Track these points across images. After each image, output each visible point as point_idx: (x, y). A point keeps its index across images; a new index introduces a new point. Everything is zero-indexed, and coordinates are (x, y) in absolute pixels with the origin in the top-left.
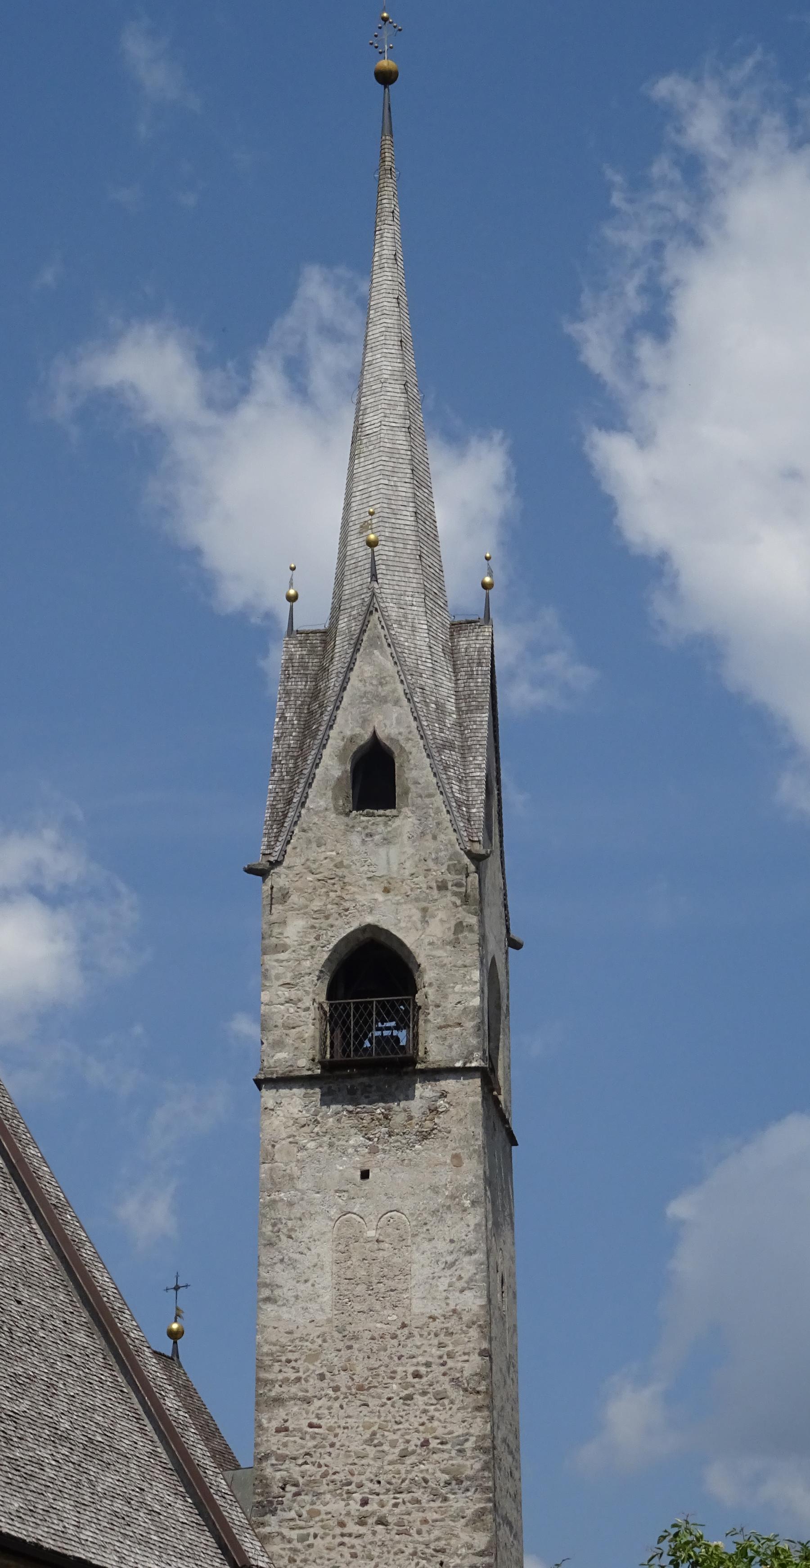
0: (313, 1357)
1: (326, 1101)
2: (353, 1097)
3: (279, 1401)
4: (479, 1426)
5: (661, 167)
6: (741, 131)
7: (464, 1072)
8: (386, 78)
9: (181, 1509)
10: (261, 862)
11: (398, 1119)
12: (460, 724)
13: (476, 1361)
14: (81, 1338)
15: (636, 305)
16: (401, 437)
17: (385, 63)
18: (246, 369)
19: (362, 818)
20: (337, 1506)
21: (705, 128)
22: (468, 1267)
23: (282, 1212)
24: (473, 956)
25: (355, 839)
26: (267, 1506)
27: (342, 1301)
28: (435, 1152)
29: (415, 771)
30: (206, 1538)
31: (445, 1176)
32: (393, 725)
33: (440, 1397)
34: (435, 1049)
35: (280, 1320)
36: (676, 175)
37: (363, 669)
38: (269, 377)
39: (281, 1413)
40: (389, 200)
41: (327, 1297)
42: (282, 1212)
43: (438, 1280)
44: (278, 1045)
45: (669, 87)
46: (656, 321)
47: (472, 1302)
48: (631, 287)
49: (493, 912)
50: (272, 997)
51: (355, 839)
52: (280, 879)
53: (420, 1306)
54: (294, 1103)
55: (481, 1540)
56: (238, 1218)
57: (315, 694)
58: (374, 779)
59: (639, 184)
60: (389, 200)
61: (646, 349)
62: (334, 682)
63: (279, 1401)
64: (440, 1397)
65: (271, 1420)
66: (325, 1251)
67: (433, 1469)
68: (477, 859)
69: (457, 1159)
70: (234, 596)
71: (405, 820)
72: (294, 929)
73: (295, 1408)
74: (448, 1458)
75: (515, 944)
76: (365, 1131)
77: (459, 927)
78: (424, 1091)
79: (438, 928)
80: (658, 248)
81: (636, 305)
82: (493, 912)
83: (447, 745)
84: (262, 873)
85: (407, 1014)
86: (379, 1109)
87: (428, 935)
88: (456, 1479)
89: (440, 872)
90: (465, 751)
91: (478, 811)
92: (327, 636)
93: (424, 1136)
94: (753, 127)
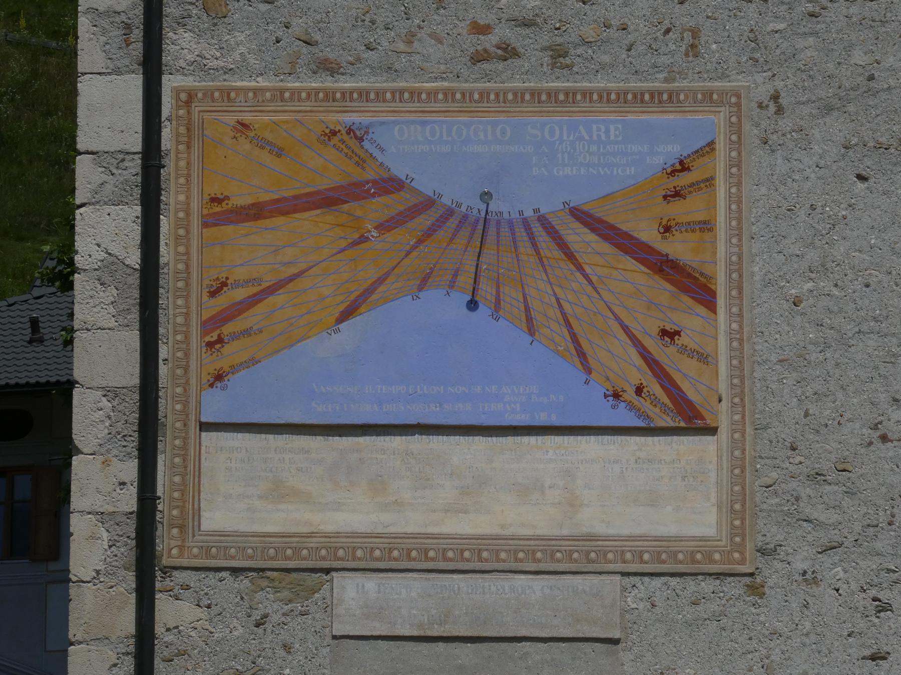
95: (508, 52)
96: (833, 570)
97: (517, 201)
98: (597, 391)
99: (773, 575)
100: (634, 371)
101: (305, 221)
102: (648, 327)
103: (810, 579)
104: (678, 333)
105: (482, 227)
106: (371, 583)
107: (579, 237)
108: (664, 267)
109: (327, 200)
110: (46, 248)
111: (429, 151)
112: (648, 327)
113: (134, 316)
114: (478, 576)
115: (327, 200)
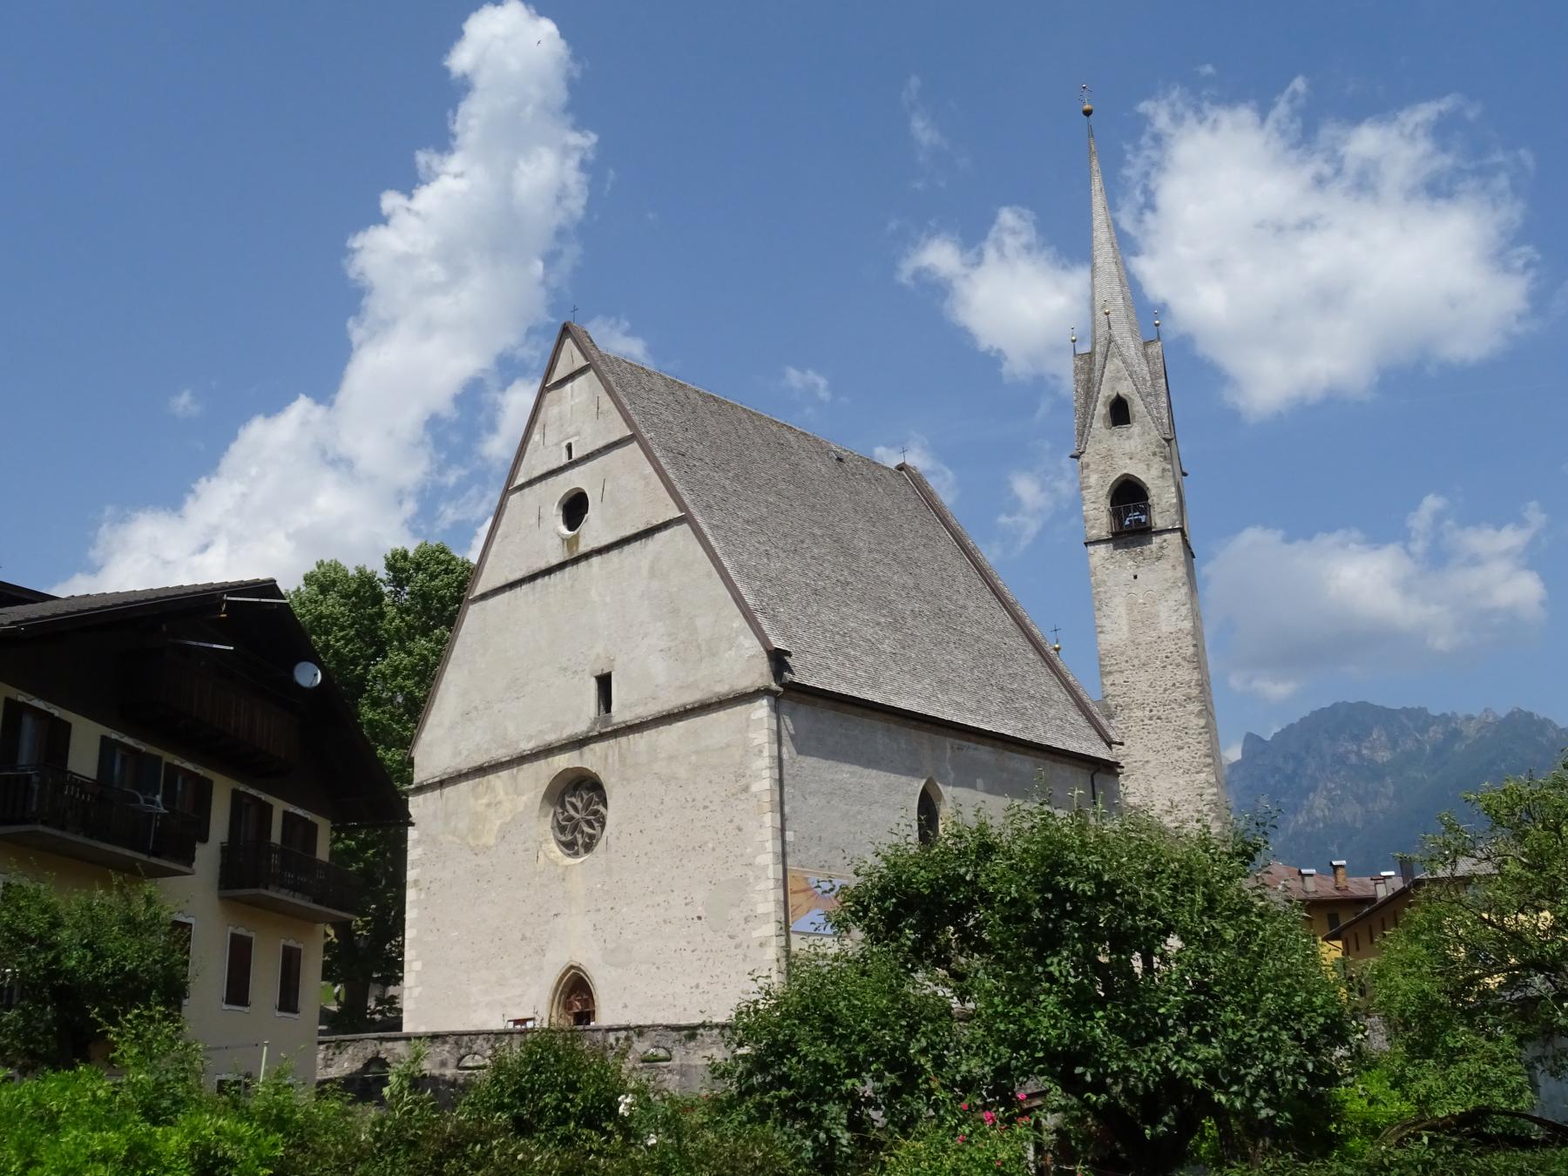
0: (1122, 654)
1: (1116, 548)
2: (1126, 546)
3: (1110, 673)
4: (1196, 676)
5: (1145, 140)
6: (1177, 119)
7: (1173, 530)
8: (1088, 113)
9: (1082, 721)
10: (1075, 452)
11: (1147, 552)
12: (1153, 385)
13: (1191, 650)
14: (1031, 656)
15: (1141, 200)
16: (1113, 267)
17: (1087, 107)
18: (981, 255)
19: (1116, 429)
20: (1139, 714)
21: (1162, 120)
22: (1184, 611)
23: (1102, 596)
24: (1171, 481)
25: (1115, 438)
26: (1110, 717)
27: (1132, 629)
28: (1163, 565)
29: (1137, 407)
30: (1093, 732)
31: (1170, 574)
32: (1125, 389)
33: (1178, 665)
34: (1159, 521)
35: (1106, 640)
36: (1151, 143)
37: (1110, 367)
38: (991, 254)
39: (1111, 678)
40: (1095, 165)
41: (1125, 629)
42: (1102, 596)
43: (1171, 616)
44: (1092, 527)
45: (1145, 107)
46: (1150, 205)
47: (1187, 625)
48: (1137, 192)
49: (1176, 462)
50: (1088, 508)
51: (1115, 438)
52: (1085, 459)
53: (1165, 628)
54: (1102, 551)
55: (1202, 722)
56: (1087, 602)
57: (1089, 380)
58: (1120, 412)
59: (1138, 148)
60: (1095, 165)
61: (1148, 216)
62: (1097, 374)
63: (1110, 673)
64: (1178, 665)
65: (1108, 681)
66: (1122, 610)
67: (1178, 695)
68: (1168, 441)
69: (1174, 567)
70: (984, 344)
71: (1135, 429)
72: (1093, 479)
73: (1117, 675)
74: (1185, 690)
75: (1185, 474)
76: (1133, 559)
77: (1164, 470)
78: (1156, 540)
79: (1155, 471)
80: (1147, 175)
81: (1141, 200)
82: (1176, 462)
83: (1149, 394)
84: (1077, 457)
85: (1146, 510)
86: (1138, 549)
87: (1150, 475)
88: (1189, 698)
89: (1153, 448)
90: (1157, 396)
91: (1165, 420)
92: (1091, 354)
93: (1159, 559)
94: (1182, 117)
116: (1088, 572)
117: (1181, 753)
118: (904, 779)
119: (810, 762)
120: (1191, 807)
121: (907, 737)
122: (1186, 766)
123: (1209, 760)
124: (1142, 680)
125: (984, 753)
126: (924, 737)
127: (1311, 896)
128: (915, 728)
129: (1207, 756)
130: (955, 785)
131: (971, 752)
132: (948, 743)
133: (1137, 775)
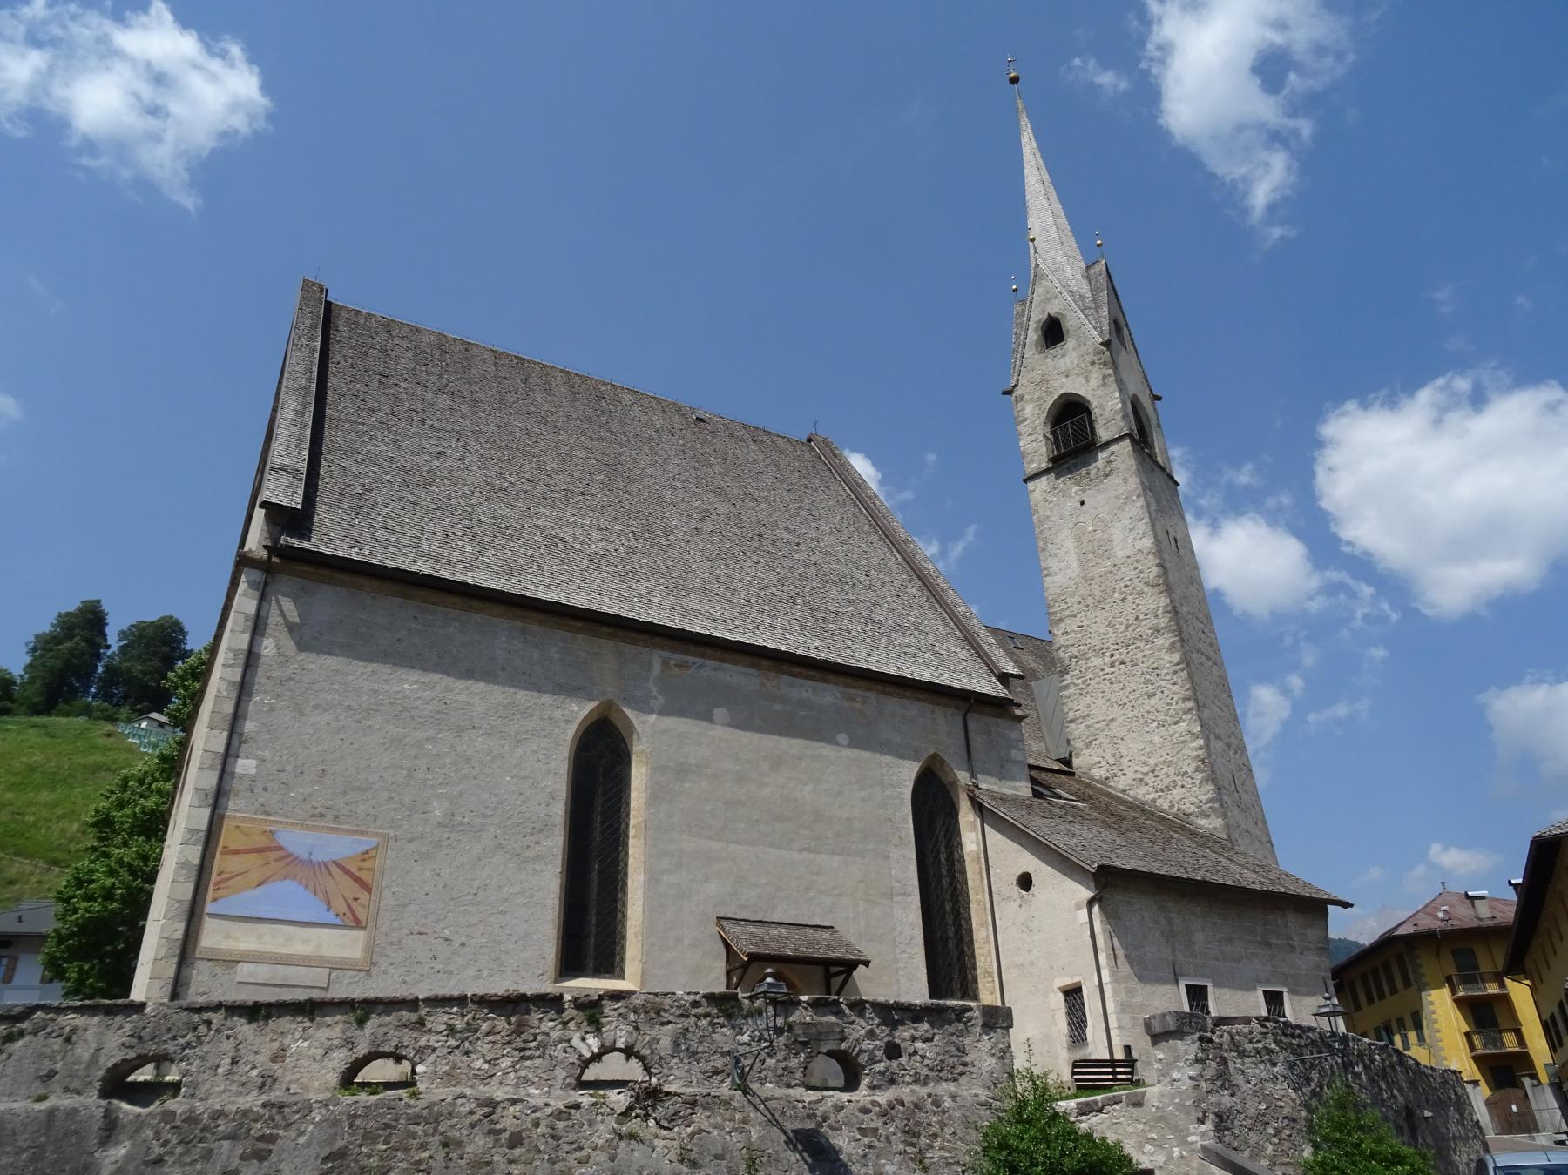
2: (1070, 471)
7: (1120, 438)
8: (1014, 81)
12: (1094, 300)
20: (1098, 662)
23: (1047, 534)
25: (1049, 361)
27: (1082, 563)
35: (1053, 584)
39: (1063, 625)
40: (1025, 121)
44: (1032, 461)
52: (1018, 392)
53: (1120, 553)
54: (1043, 483)
60: (1025, 121)
63: (1061, 620)
66: (1070, 545)
71: (1070, 343)
73: (1068, 621)
74: (1150, 622)
75: (1158, 398)
77: (1104, 377)
86: (1083, 471)
88: (1157, 631)
90: (1097, 308)
93: (1107, 475)
95: (322, 815)
96: (392, 970)
97: (319, 857)
98: (332, 913)
99: (374, 971)
100: (344, 909)
101: (250, 856)
102: (350, 898)
103: (385, 972)
104: (849, 966)
105: (311, 864)
106: (252, 966)
107: (334, 869)
108: (357, 880)
109: (259, 851)
110: (1161, 1056)
111: (296, 840)
112: (350, 898)
113: (193, 879)
114: (963, 742)
115: (259, 851)
116: (1026, 509)
117: (1153, 701)
118: (547, 699)
119: (322, 665)
120: (1172, 770)
121: (557, 644)
122: (1161, 717)
123: (1190, 704)
124: (1097, 621)
125: (736, 675)
126: (581, 643)
127: (1484, 924)
128: (609, 636)
129: (1186, 699)
130: (663, 712)
131: (704, 673)
132: (656, 659)
133: (1102, 739)
